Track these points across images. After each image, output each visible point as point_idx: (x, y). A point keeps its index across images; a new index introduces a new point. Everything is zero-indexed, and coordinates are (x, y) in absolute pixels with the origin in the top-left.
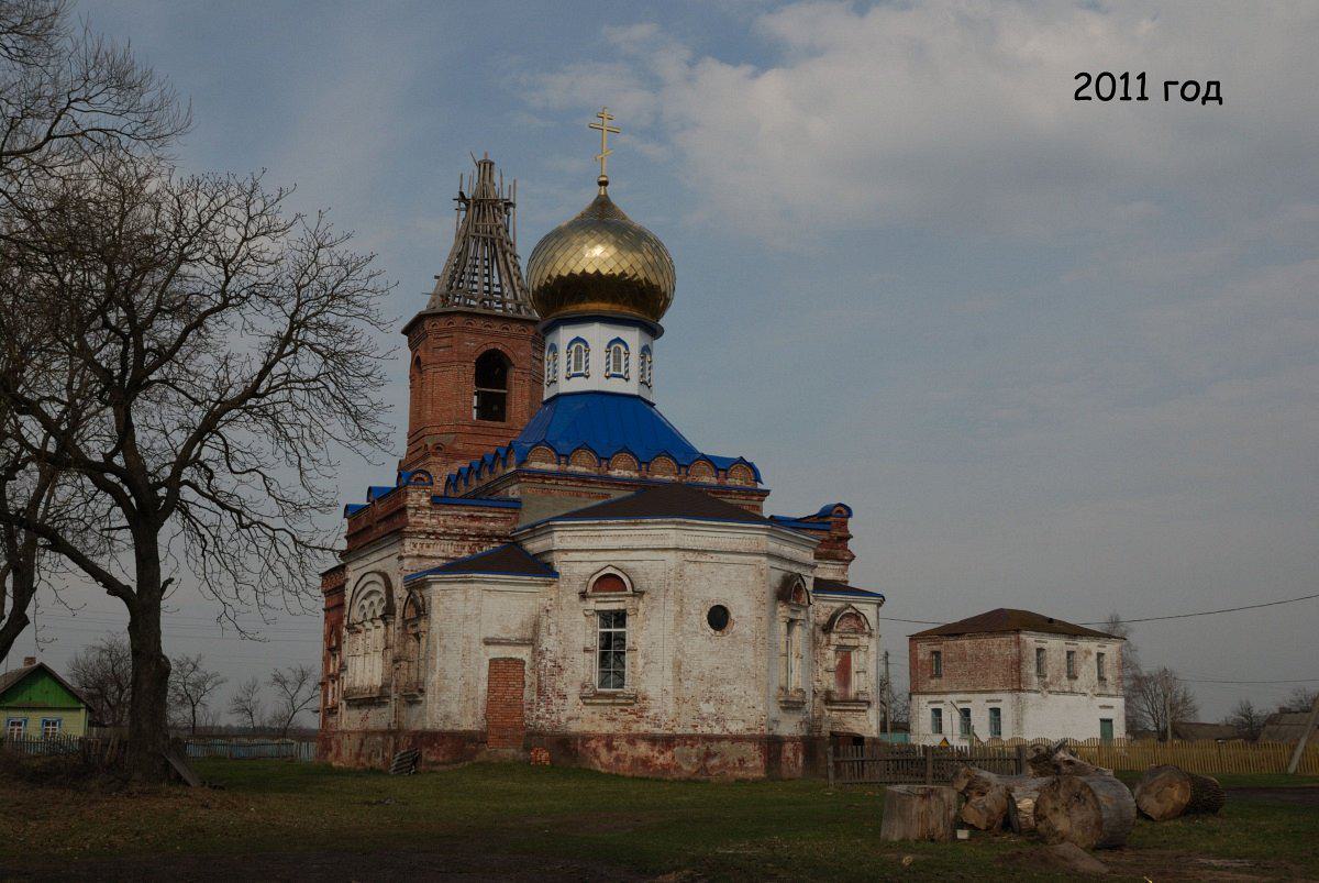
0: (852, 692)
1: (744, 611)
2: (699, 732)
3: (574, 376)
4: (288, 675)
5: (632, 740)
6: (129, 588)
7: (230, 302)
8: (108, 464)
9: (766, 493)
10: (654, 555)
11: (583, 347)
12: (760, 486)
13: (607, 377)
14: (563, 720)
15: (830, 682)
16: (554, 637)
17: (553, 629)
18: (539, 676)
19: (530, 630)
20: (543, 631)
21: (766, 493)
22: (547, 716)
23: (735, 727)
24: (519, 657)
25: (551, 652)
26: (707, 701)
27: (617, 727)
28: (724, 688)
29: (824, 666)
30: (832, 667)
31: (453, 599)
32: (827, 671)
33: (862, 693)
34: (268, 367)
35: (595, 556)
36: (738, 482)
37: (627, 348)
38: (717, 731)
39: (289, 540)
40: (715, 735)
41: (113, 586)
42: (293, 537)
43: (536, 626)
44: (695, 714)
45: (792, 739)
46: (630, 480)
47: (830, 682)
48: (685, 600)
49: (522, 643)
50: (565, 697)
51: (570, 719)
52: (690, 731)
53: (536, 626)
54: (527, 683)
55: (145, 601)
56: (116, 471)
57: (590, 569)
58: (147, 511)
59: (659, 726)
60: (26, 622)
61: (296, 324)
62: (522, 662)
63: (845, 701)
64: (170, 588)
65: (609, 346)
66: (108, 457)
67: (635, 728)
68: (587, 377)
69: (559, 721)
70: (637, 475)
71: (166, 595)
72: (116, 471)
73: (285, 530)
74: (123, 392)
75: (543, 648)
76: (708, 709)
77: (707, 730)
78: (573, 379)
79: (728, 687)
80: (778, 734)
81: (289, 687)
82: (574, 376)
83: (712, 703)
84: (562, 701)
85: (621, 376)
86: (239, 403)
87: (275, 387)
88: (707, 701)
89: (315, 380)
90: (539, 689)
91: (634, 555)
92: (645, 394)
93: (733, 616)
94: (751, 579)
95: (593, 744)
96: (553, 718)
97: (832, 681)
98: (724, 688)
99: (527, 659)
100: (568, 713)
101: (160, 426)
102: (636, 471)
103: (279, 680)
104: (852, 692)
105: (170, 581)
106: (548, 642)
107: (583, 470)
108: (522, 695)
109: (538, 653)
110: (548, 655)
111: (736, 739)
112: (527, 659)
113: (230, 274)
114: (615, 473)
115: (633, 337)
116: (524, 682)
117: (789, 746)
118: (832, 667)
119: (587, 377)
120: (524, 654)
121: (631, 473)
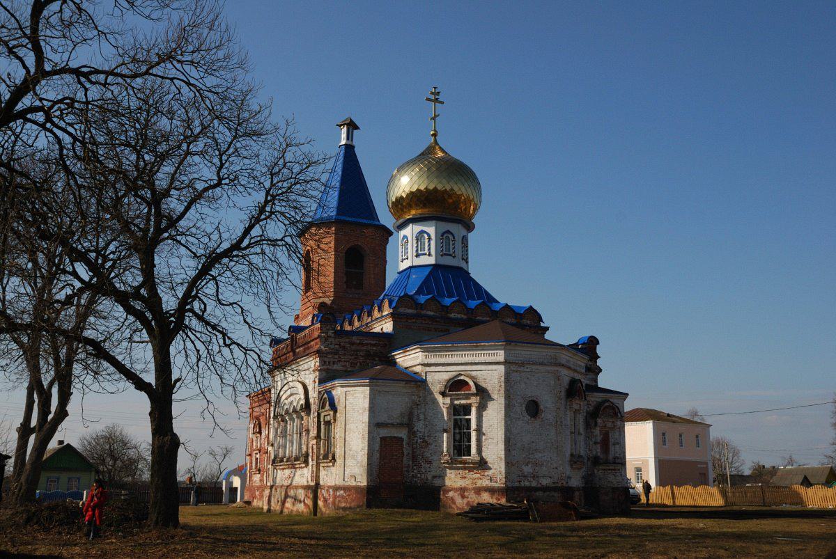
0: (611, 457)
1: (548, 402)
2: (523, 485)
3: (445, 254)
4: (217, 450)
5: (478, 491)
6: (150, 384)
7: (223, 182)
8: (136, 294)
9: (547, 329)
10: (483, 367)
11: (451, 237)
12: (542, 324)
13: (442, 255)
14: (430, 478)
15: (598, 450)
16: (422, 422)
17: (422, 417)
18: (413, 449)
19: (406, 418)
20: (415, 419)
21: (547, 329)
22: (419, 475)
23: (545, 482)
24: (400, 436)
25: (420, 432)
26: (527, 465)
27: (467, 482)
28: (538, 455)
29: (593, 440)
30: (599, 441)
31: (355, 398)
32: (595, 443)
33: (618, 458)
34: (247, 231)
35: (449, 368)
36: (529, 322)
37: (454, 238)
38: (534, 484)
39: (256, 357)
40: (533, 487)
41: (140, 385)
42: (259, 356)
43: (411, 415)
44: (520, 473)
45: (578, 489)
46: (462, 319)
47: (598, 450)
48: (511, 397)
49: (401, 425)
50: (430, 463)
51: (434, 477)
52: (517, 484)
53: (411, 415)
54: (405, 454)
55: (161, 397)
56: (141, 298)
57: (446, 376)
58: (163, 330)
59: (496, 482)
60: (66, 414)
61: (271, 198)
62: (401, 439)
63: (607, 462)
64: (178, 384)
65: (442, 235)
66: (138, 289)
67: (480, 483)
68: (454, 257)
69: (427, 479)
70: (465, 317)
71: (175, 390)
72: (141, 298)
73: (254, 351)
74: (146, 250)
75: (415, 429)
76: (527, 469)
77: (527, 484)
78: (446, 257)
79: (540, 455)
80: (570, 485)
81: (218, 457)
82: (445, 254)
83: (530, 466)
84: (429, 465)
85: (450, 255)
86: (227, 253)
87: (253, 243)
88: (527, 465)
89: (282, 240)
90: (413, 457)
91: (479, 367)
92: (463, 265)
93: (541, 407)
94: (552, 382)
95: (451, 494)
96: (423, 477)
97: (599, 450)
98: (538, 455)
99: (405, 437)
100: (433, 473)
101: (175, 265)
102: (465, 315)
103: (213, 454)
104: (611, 457)
105: (178, 380)
106: (419, 426)
107: (432, 313)
108: (402, 461)
109: (412, 433)
110: (419, 435)
111: (545, 489)
112: (405, 437)
113: (224, 162)
114: (452, 315)
115: (454, 228)
116: (403, 453)
117: (577, 494)
118: (599, 441)
119: (454, 257)
120: (403, 434)
121: (462, 316)
